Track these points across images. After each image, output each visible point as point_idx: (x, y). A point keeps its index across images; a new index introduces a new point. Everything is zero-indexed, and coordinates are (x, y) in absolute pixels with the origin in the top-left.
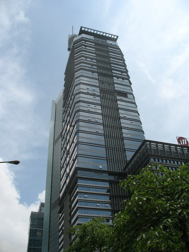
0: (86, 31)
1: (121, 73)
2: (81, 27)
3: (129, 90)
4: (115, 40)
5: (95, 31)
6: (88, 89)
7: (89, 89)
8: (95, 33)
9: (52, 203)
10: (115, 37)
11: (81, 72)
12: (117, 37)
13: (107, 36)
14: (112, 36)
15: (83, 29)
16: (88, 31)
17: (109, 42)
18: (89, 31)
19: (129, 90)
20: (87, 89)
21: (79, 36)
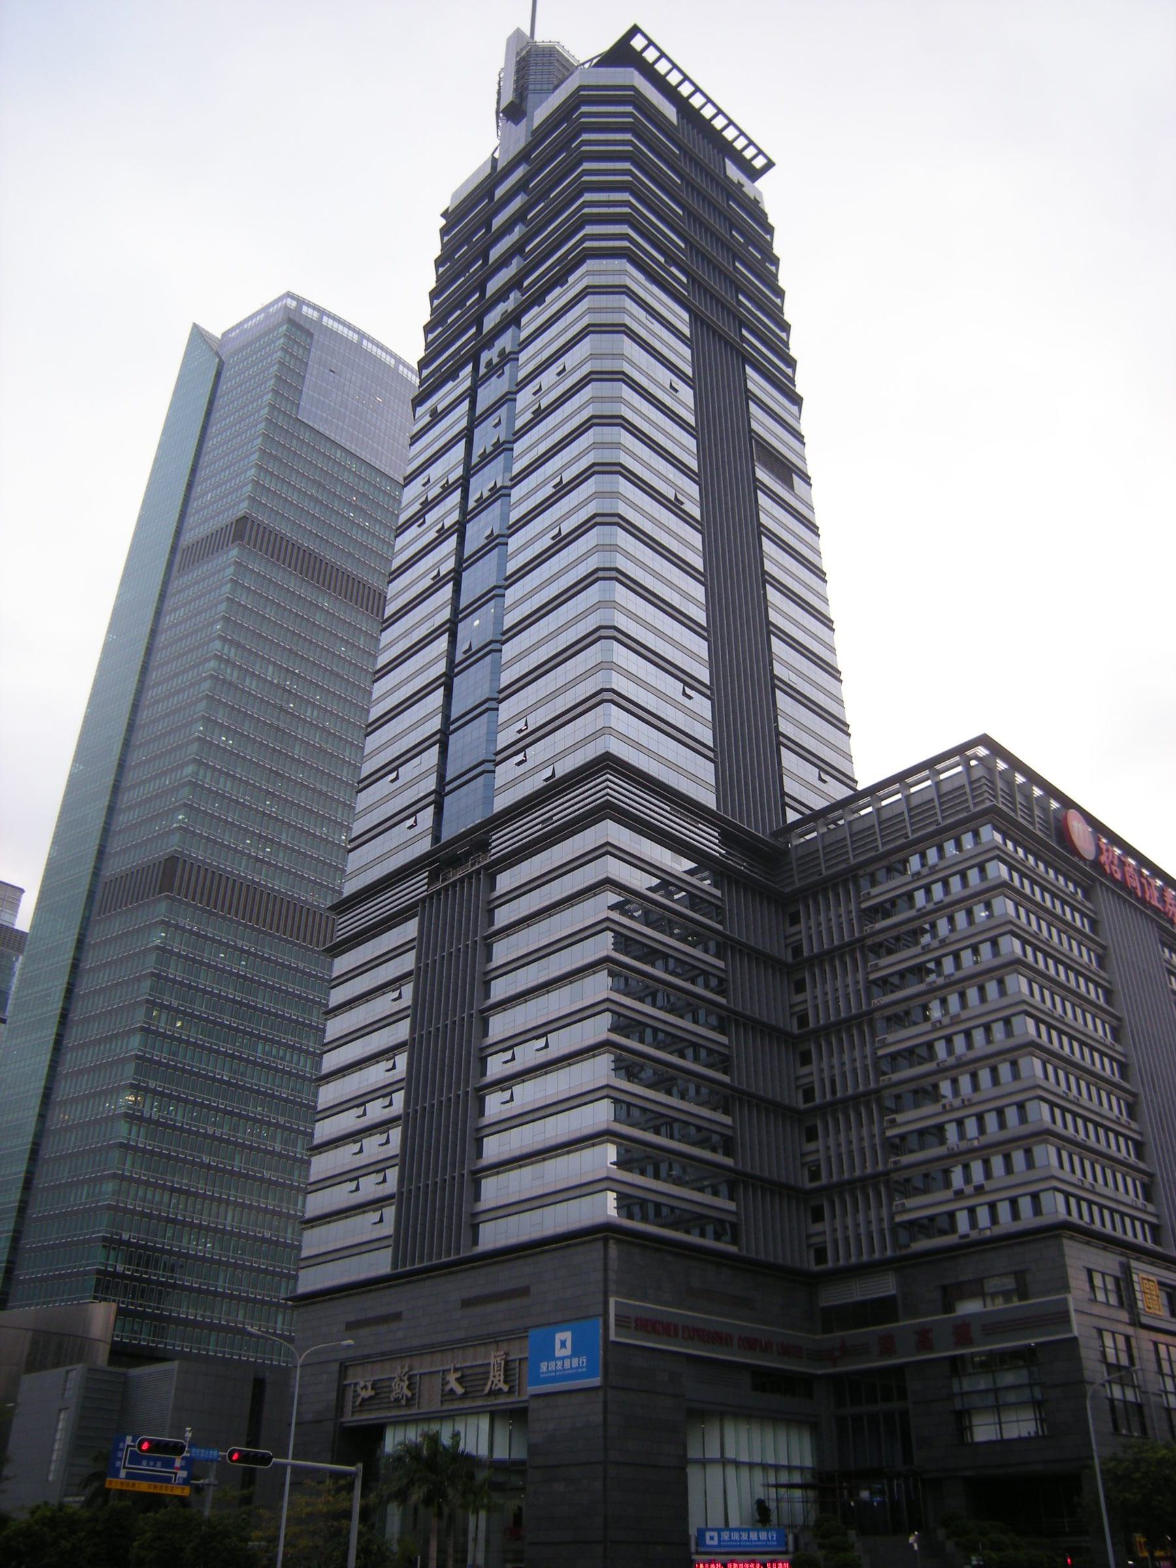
0: (745, 158)
1: (665, 261)
2: (635, 30)
3: (791, 414)
4: (754, 174)
5: (651, 48)
6: (676, 391)
7: (677, 394)
8: (713, 128)
9: (188, 538)
10: (759, 163)
11: (588, 273)
12: (770, 165)
13: (631, 46)
14: (686, 83)
15: (638, 43)
16: (679, 89)
17: (733, 173)
18: (662, 67)
19: (791, 414)
20: (668, 387)
21: (595, 69)
